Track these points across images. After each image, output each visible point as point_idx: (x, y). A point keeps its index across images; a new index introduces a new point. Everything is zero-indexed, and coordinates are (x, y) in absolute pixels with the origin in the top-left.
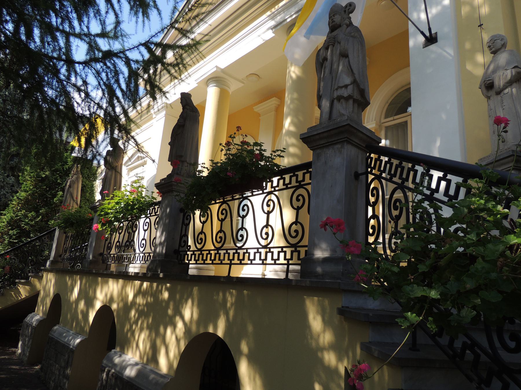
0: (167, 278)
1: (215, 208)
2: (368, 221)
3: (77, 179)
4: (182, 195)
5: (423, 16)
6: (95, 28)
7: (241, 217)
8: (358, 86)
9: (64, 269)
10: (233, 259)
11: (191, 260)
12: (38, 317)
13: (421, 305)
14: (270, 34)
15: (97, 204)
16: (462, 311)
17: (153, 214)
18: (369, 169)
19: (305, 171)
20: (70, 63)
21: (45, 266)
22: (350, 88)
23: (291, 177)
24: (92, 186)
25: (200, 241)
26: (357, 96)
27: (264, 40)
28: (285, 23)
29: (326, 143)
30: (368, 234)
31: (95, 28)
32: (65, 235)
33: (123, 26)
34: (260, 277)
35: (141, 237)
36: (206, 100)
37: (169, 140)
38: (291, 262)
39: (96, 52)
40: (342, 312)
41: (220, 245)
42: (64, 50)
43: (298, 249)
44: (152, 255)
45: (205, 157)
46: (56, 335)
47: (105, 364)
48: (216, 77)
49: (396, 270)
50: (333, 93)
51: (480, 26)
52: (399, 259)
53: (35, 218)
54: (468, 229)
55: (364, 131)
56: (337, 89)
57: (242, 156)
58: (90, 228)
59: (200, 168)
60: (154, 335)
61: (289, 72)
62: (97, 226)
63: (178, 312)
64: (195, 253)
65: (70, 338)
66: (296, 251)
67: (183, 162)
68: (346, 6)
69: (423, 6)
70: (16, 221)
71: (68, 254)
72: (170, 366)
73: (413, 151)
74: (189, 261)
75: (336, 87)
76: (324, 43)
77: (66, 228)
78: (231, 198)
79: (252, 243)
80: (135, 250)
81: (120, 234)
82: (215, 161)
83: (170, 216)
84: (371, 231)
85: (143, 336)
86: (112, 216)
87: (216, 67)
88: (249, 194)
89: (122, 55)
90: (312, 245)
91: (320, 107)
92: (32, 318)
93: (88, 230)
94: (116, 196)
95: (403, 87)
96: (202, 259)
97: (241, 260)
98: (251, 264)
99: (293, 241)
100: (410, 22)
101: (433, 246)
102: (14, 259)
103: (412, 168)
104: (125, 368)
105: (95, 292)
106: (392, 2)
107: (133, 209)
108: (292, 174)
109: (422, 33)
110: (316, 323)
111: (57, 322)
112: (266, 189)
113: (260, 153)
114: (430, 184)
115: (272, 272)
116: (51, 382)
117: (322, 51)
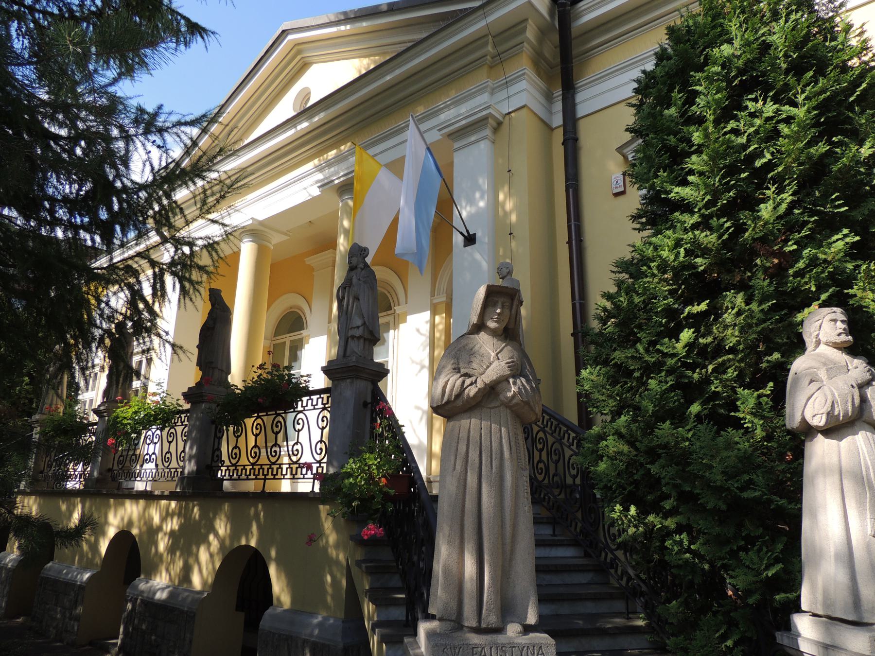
14: (316, 192)
17: (179, 423)
22: (361, 328)
26: (367, 335)
28: (331, 184)
45: (236, 377)
46: (52, 574)
51: (511, 234)
63: (212, 529)
67: (213, 368)
72: (204, 583)
87: (252, 218)
97: (274, 475)
104: (155, 594)
109: (462, 233)
110: (328, 525)
111: (51, 559)
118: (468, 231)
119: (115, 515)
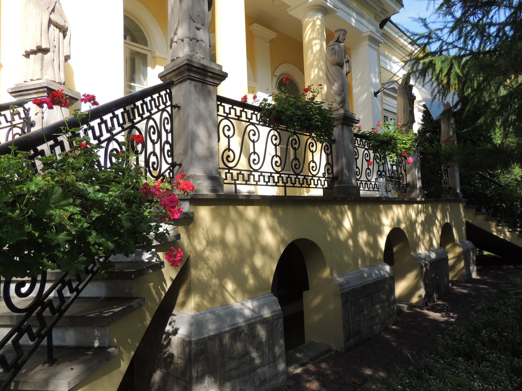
105: (379, 219)
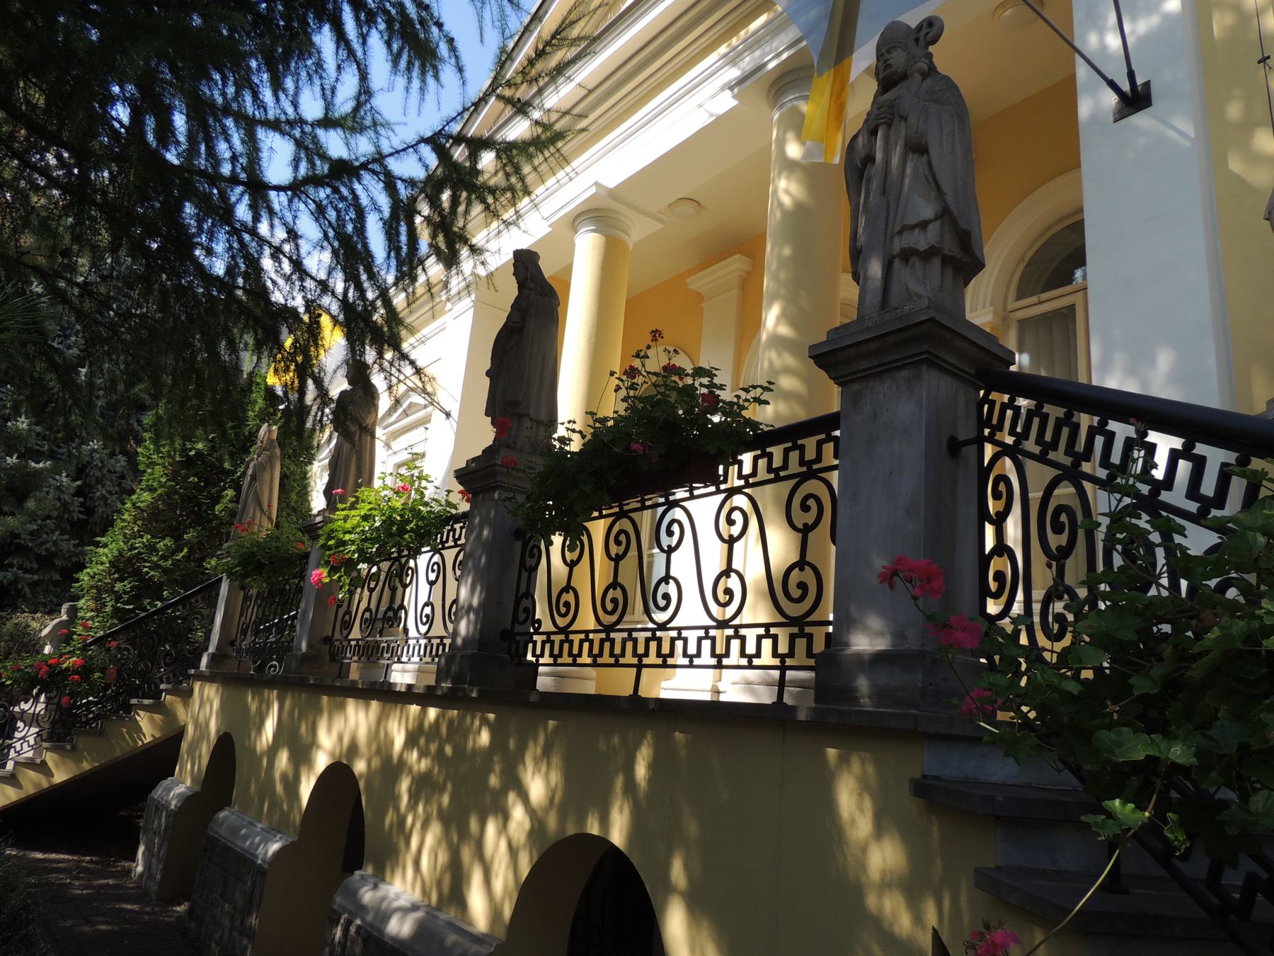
0: (490, 699)
1: (598, 528)
2: (985, 561)
3: (271, 459)
4: (520, 498)
5: (1113, 41)
6: (312, 108)
7: (662, 550)
8: (954, 223)
9: (244, 673)
10: (646, 654)
11: (542, 655)
12: (180, 789)
13: (1142, 780)
14: (727, 102)
15: (319, 519)
16: (1253, 799)
17: (451, 543)
18: (987, 431)
19: (823, 436)
20: (258, 189)
21: (197, 666)
23: (786, 452)
24: (304, 476)
25: (563, 610)
26: (951, 247)
27: (711, 115)
29: (876, 367)
30: (985, 593)
31: (312, 108)
32: (242, 593)
33: (379, 101)
34: (707, 697)
35: (423, 599)
36: (571, 264)
37: (487, 365)
38: (789, 662)
39: (318, 163)
40: (924, 789)
41: (614, 618)
42: (243, 161)
43: (808, 630)
44: (447, 642)
45: (573, 402)
47: (340, 906)
48: (596, 210)
49: (1073, 688)
50: (892, 241)
51: (1264, 60)
52: (1080, 661)
53: (173, 553)
54: (1263, 588)
55: (972, 336)
56: (900, 233)
57: (666, 402)
58: (302, 576)
59: (561, 431)
60: (455, 838)
61: (775, 192)
62: (319, 574)
64: (553, 637)
65: (257, 839)
66: (802, 634)
67: (520, 416)
68: (920, 27)
69: (1113, 18)
70: (129, 560)
71: (249, 638)
72: (495, 914)
73: (1095, 383)
74: (537, 657)
75: (898, 228)
76: (866, 121)
77: (244, 576)
78: (639, 505)
79: (692, 614)
80: (406, 630)
81: (371, 590)
82: (600, 415)
83: (490, 547)
84: (993, 586)
85: (430, 840)
86: (353, 548)
87: (596, 184)
88: (680, 494)
89: (377, 167)
90: (846, 621)
91: (856, 277)
92: (169, 790)
93: (296, 581)
94: (363, 501)
95: (1060, 220)
96: (570, 654)
97: (665, 657)
98: (691, 666)
99: (795, 610)
100: (1079, 59)
101: (1166, 628)
102: (126, 649)
103: (1101, 429)
104: (385, 917)
105: (313, 730)
106: (1029, 5)
107: (402, 531)
108: (789, 444)
109: (1112, 85)
111: (226, 802)
112: (725, 481)
113: (711, 392)
114: (1150, 464)
115: (736, 687)
116: (213, 945)
117: (860, 140)
118: (1131, 75)
119: (329, 729)
